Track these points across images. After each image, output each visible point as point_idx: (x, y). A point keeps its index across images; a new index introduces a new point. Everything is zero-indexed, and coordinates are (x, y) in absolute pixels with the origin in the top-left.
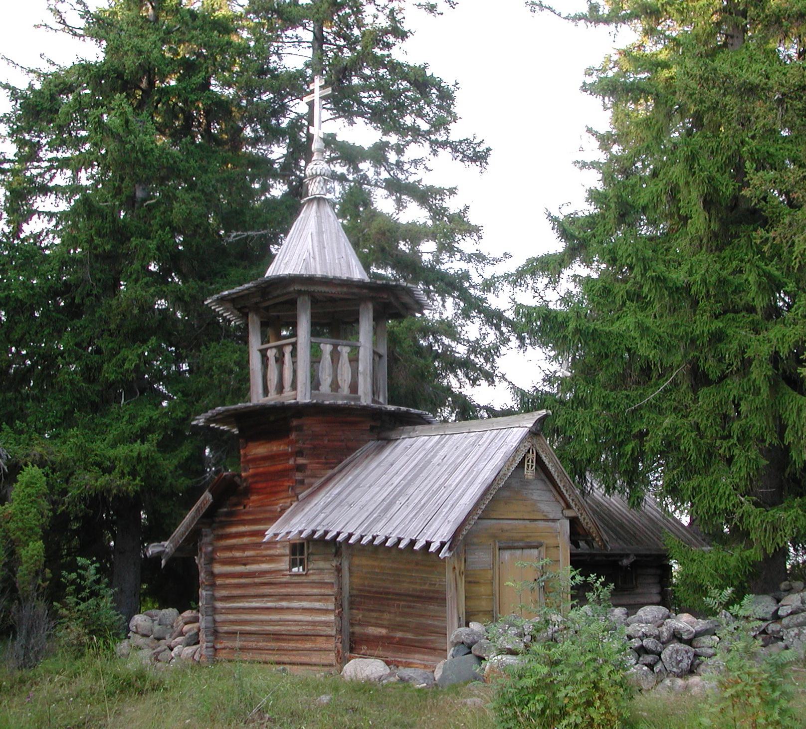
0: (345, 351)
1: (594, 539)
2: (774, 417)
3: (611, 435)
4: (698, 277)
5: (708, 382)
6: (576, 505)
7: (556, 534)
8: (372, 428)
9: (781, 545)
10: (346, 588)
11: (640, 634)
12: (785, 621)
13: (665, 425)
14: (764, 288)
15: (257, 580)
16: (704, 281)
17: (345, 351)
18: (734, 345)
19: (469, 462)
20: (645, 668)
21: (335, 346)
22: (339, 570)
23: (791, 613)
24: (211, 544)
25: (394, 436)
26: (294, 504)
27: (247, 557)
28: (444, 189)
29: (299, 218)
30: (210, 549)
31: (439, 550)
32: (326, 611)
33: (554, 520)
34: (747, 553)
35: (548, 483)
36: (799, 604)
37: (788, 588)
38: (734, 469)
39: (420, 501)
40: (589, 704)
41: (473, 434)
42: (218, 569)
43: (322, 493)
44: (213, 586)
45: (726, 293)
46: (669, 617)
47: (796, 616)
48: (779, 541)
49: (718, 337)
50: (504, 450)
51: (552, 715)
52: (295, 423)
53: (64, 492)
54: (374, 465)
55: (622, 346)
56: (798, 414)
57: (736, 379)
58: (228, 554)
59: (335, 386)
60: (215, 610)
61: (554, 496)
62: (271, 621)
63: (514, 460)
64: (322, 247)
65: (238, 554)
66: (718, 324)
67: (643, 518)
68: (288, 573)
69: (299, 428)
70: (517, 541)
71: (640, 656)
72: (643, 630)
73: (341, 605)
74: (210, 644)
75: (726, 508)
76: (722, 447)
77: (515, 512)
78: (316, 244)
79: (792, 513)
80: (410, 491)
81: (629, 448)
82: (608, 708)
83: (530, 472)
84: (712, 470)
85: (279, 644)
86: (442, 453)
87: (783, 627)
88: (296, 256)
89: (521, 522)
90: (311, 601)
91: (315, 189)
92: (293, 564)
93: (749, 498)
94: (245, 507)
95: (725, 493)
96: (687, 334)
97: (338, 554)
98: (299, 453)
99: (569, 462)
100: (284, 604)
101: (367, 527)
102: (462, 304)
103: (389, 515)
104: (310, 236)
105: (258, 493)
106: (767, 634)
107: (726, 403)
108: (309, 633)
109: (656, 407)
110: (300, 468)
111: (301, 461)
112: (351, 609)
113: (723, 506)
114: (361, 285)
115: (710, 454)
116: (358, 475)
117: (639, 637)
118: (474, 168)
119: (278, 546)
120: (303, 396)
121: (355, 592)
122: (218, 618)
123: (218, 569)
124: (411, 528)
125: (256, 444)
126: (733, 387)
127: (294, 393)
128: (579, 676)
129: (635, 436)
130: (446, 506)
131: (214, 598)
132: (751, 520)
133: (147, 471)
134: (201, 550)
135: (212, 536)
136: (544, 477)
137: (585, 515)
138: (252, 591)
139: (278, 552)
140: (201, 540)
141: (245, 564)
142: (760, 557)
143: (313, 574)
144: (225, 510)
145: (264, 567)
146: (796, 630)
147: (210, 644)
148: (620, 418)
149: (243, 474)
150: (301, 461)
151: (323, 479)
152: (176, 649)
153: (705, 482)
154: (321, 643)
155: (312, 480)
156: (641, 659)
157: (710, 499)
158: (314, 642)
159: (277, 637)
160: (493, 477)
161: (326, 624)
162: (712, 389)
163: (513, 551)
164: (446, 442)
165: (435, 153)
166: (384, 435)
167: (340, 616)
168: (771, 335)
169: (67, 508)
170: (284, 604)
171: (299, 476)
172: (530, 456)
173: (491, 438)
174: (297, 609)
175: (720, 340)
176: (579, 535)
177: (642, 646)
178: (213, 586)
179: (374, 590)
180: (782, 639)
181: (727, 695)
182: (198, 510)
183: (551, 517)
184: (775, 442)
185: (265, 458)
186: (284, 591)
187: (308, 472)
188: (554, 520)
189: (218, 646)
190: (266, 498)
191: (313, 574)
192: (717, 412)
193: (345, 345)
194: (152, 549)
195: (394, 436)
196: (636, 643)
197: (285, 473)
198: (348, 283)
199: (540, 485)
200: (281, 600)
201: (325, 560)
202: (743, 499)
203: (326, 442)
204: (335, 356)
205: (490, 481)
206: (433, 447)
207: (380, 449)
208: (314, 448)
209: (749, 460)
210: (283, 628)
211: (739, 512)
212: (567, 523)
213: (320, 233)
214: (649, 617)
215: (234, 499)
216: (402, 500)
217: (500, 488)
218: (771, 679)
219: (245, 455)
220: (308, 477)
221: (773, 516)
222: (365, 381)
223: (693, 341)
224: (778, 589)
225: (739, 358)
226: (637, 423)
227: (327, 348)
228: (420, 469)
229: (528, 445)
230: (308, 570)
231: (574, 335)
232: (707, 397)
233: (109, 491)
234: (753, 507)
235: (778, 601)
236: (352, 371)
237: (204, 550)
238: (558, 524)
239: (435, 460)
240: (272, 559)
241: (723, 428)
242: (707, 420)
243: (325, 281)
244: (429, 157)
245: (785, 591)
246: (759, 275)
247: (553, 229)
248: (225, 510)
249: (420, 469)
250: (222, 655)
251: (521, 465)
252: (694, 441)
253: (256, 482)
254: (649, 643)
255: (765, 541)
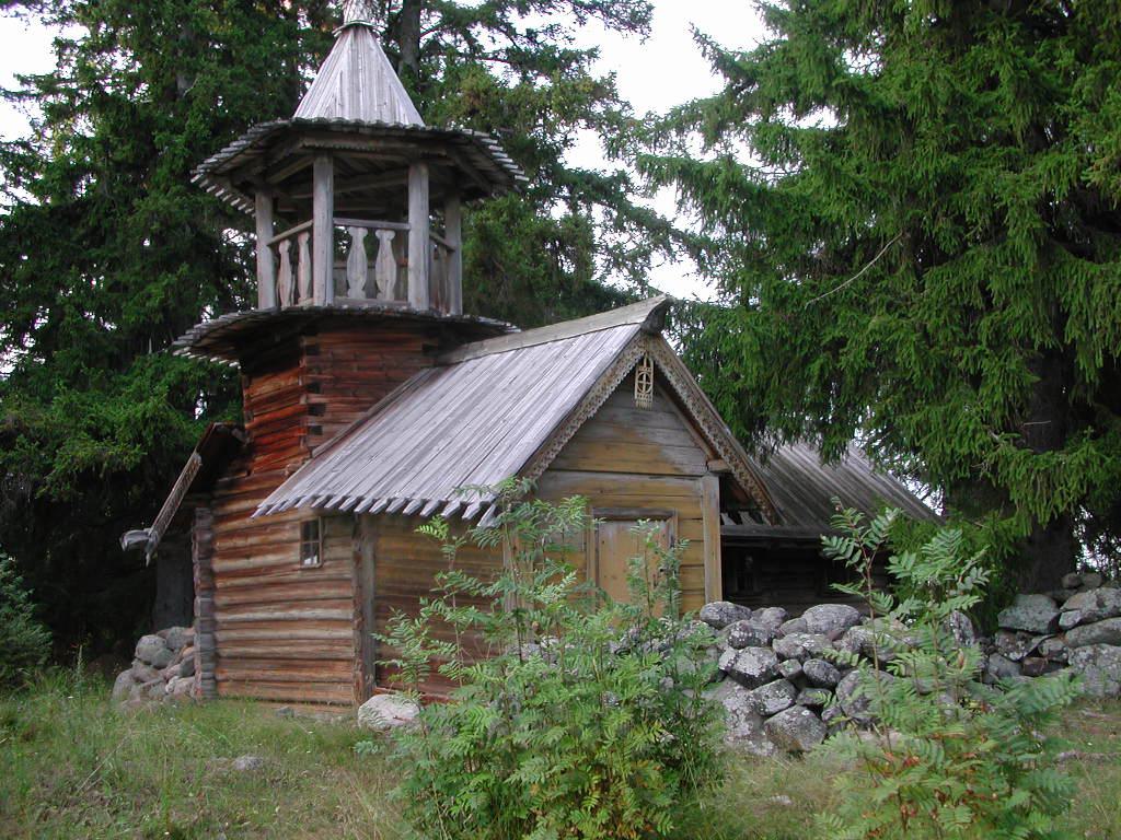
0: (386, 237)
1: (759, 508)
2: (1046, 301)
3: (787, 347)
4: (917, 89)
5: (944, 258)
6: (726, 451)
7: (697, 499)
8: (426, 350)
9: (1061, 509)
10: (370, 586)
11: (799, 651)
12: (1071, 636)
13: (870, 326)
14: (1026, 92)
15: (262, 579)
16: (927, 93)
17: (386, 237)
18: (980, 191)
19: (547, 381)
20: (806, 713)
21: (371, 230)
22: (358, 558)
23: (1081, 623)
24: (209, 529)
25: (455, 359)
26: (307, 462)
27: (252, 545)
28: (582, 53)
29: (329, 58)
30: (208, 536)
31: (478, 516)
32: (343, 623)
33: (693, 477)
34: (1005, 524)
35: (682, 418)
36: (1093, 606)
37: (1075, 584)
38: (983, 391)
39: (465, 445)
40: (576, 798)
41: (561, 342)
42: (219, 565)
43: (344, 446)
44: (212, 589)
45: (965, 116)
46: (859, 623)
47: (1089, 627)
48: (1059, 502)
49: (952, 183)
50: (598, 359)
51: (506, 817)
52: (305, 342)
53: (48, 469)
54: (418, 401)
55: (807, 215)
56: (1088, 294)
57: (984, 249)
58: (230, 543)
59: (372, 289)
60: (214, 625)
61: (693, 440)
62: (280, 639)
63: (614, 374)
64: (355, 90)
65: (240, 542)
66: (949, 160)
67: (861, 493)
68: (299, 566)
69: (313, 351)
70: (629, 508)
71: (798, 691)
72: (806, 645)
73: (361, 612)
74: (208, 674)
75: (971, 454)
76: (964, 358)
77: (624, 461)
78: (346, 85)
79: (1077, 458)
80: (456, 431)
81: (815, 367)
82: (616, 816)
83: (643, 397)
84: (947, 395)
85: (289, 673)
86: (512, 374)
87: (1066, 645)
88: (319, 105)
89: (634, 478)
90: (326, 608)
91: (351, 13)
92: (306, 553)
93: (1008, 436)
94: (249, 474)
95: (967, 429)
96: (902, 179)
97: (356, 534)
98: (313, 388)
99: (731, 398)
100: (295, 613)
101: (388, 484)
102: (615, 214)
103: (417, 468)
104: (339, 76)
105: (264, 452)
106: (1041, 656)
107: (969, 288)
108: (327, 656)
109: (858, 304)
110: (314, 410)
111: (315, 399)
112: (377, 618)
113: (965, 450)
114: (409, 134)
115: (945, 371)
116: (393, 418)
117: (798, 658)
118: (636, 36)
119: (287, 527)
120: (321, 298)
121: (381, 592)
122: (221, 636)
123: (219, 565)
124: (444, 483)
125: (262, 379)
126: (980, 259)
127: (310, 300)
128: (553, 735)
129: (826, 348)
130: (500, 448)
131: (213, 608)
132: (1011, 469)
133: (156, 438)
134: (195, 538)
135: (211, 517)
136: (674, 409)
137: (741, 469)
138: (258, 596)
139: (286, 536)
140: (194, 524)
141: (248, 557)
142: (1026, 532)
143: (329, 567)
144: (226, 479)
145: (271, 559)
146: (1089, 650)
147: (208, 674)
148: (801, 321)
149: (247, 425)
150: (315, 399)
151: (350, 426)
152: (171, 682)
153: (936, 413)
154: (341, 671)
155: (335, 427)
156: (801, 696)
157: (944, 440)
158: (331, 669)
159: (287, 662)
160: (576, 399)
161: (346, 641)
162: (947, 268)
163: (622, 524)
164: (523, 357)
165: (582, 21)
166: (443, 358)
167: (361, 629)
168: (1040, 169)
169: (49, 490)
170: (295, 613)
171: (312, 421)
172: (644, 370)
173: (583, 345)
174: (312, 620)
175: (956, 188)
176: (738, 502)
177: (802, 672)
178: (212, 589)
179: (407, 587)
180: (1065, 664)
181: (879, 796)
182: (184, 479)
183: (687, 471)
184: (1050, 343)
185: (271, 400)
186: (299, 593)
187: (328, 416)
188: (693, 477)
189: (220, 677)
190: (274, 458)
191: (329, 567)
192: (954, 303)
193: (387, 229)
194: (129, 539)
195: (455, 359)
196: (790, 668)
197: (292, 421)
198: (379, 131)
199: (667, 420)
200: (291, 607)
201: (345, 544)
202: (997, 437)
203: (355, 371)
204: (372, 246)
205: (569, 407)
206: (502, 367)
207: (433, 378)
208: (337, 380)
209: (1007, 375)
210: (294, 649)
211: (990, 458)
212: (715, 482)
213: (354, 71)
214: (821, 623)
215: (236, 464)
216: (442, 444)
217: (589, 421)
218: (1004, 757)
219: (249, 398)
220: (327, 422)
221: (1048, 462)
222: (417, 278)
223: (912, 194)
224: (1061, 587)
225: (988, 213)
226: (828, 329)
227: (359, 234)
228: (476, 399)
229: (639, 353)
230: (325, 561)
231: (726, 192)
232: (938, 282)
233: (99, 465)
234: (1014, 449)
235: (1059, 603)
236: (404, 267)
237: (198, 538)
238: (699, 484)
239: (501, 385)
240: (280, 547)
241: (966, 331)
242: (938, 316)
243: (354, 130)
244: (573, 26)
245: (1070, 588)
246: (1015, 67)
247: (704, 55)
248: (226, 479)
249: (476, 399)
250: (224, 690)
251: (627, 385)
252: (917, 349)
253: (262, 436)
254: (812, 668)
255: (1034, 504)
